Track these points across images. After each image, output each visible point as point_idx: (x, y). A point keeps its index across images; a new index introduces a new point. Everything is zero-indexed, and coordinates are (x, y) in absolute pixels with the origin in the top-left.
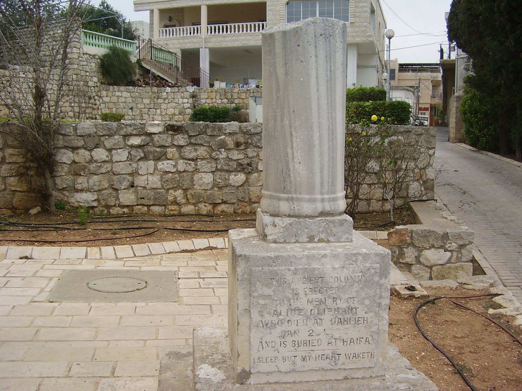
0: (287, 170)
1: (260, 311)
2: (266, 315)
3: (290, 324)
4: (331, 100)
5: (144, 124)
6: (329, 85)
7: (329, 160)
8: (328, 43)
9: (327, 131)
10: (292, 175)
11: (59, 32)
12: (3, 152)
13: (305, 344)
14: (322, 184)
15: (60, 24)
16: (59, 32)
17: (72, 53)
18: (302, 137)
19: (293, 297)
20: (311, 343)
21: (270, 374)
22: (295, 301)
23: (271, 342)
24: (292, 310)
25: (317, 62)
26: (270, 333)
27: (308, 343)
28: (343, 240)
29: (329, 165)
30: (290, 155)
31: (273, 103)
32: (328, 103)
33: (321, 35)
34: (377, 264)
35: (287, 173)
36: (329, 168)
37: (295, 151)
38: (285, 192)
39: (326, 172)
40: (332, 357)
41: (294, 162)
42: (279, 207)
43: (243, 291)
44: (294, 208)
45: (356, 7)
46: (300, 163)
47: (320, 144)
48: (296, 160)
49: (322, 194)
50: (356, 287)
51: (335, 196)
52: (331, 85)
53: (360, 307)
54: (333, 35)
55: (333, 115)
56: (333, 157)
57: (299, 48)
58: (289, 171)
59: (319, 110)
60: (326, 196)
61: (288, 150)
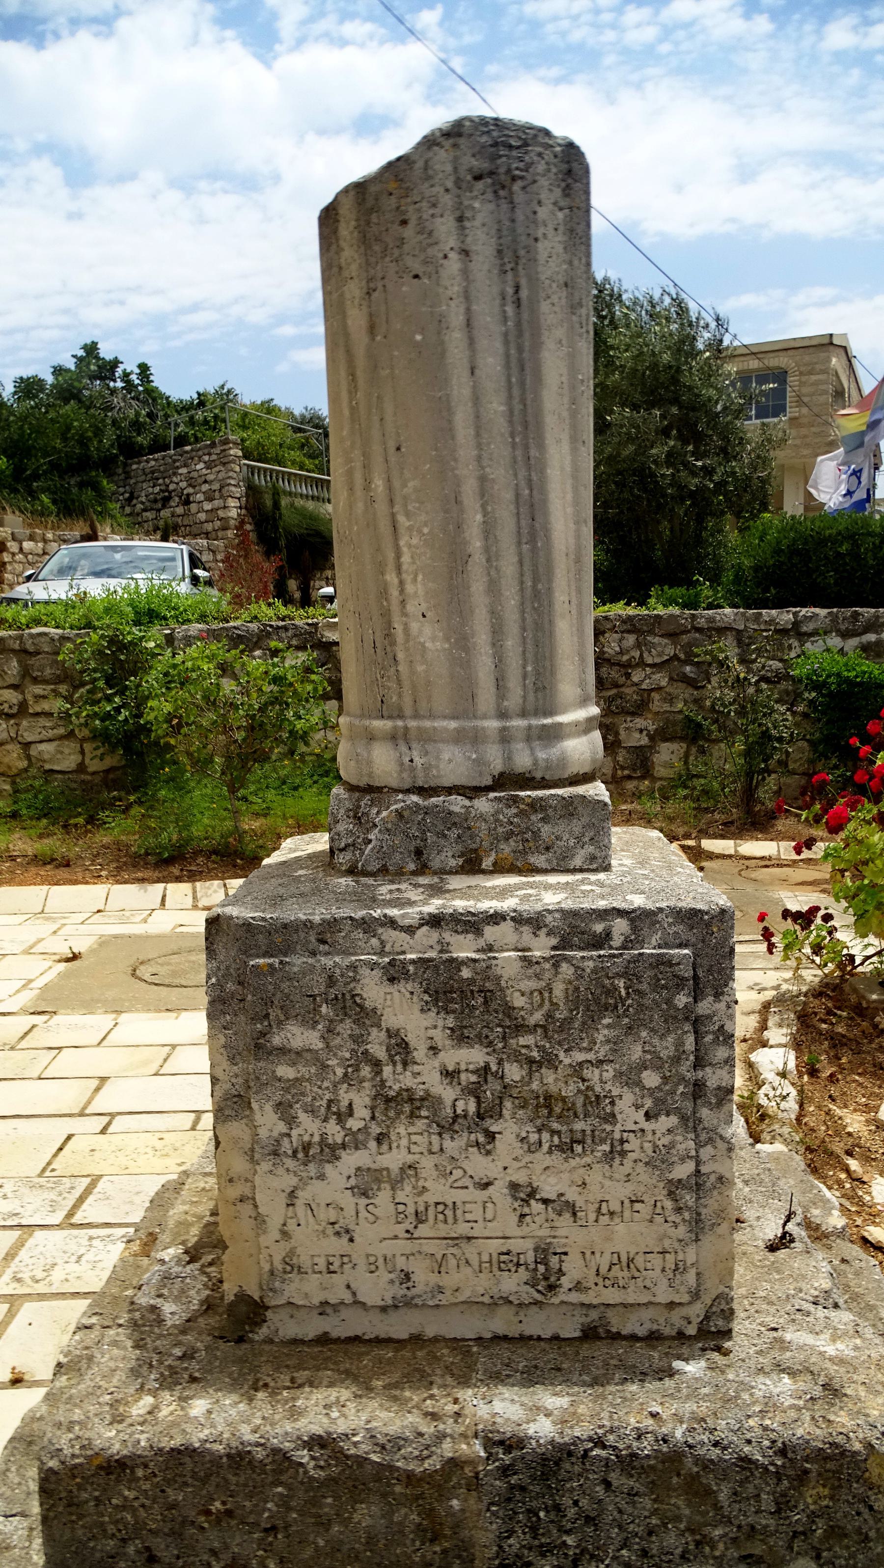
0: (386, 642)
1: (280, 1103)
2: (303, 1117)
3: (385, 1147)
4: (523, 401)
5: (315, 625)
6: (513, 352)
7: (522, 604)
8: (505, 206)
9: (512, 507)
10: (400, 656)
11: (198, 467)
12: (23, 693)
13: (441, 1217)
14: (500, 683)
15: (200, 453)
16: (198, 467)
17: (225, 507)
18: (426, 530)
19: (391, 1057)
20: (459, 1213)
21: (329, 1310)
22: (399, 1068)
23: (323, 1205)
24: (388, 1100)
25: (465, 273)
26: (321, 1177)
27: (449, 1213)
28: (577, 862)
29: (524, 620)
30: (395, 593)
31: (345, 433)
32: (511, 411)
33: (478, 178)
34: (680, 946)
35: (388, 649)
36: (524, 629)
37: (406, 577)
38: (385, 713)
39: (511, 643)
40: (536, 1262)
41: (406, 615)
42: (369, 762)
43: (225, 1036)
44: (411, 761)
45: (802, 384)
46: (424, 616)
47: (487, 549)
48: (410, 608)
49: (503, 715)
50: (608, 1026)
51: (548, 721)
52: (520, 349)
53: (628, 1098)
54: (522, 178)
55: (533, 452)
56: (536, 594)
57: (409, 232)
58: (393, 643)
59: (478, 435)
60: (519, 723)
61: (388, 577)
